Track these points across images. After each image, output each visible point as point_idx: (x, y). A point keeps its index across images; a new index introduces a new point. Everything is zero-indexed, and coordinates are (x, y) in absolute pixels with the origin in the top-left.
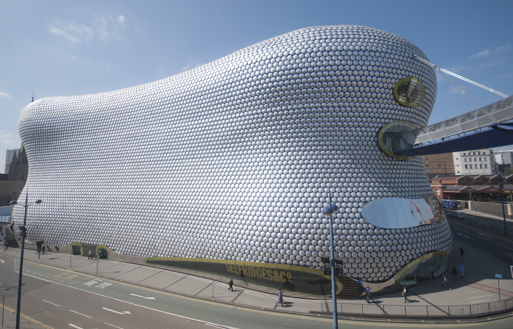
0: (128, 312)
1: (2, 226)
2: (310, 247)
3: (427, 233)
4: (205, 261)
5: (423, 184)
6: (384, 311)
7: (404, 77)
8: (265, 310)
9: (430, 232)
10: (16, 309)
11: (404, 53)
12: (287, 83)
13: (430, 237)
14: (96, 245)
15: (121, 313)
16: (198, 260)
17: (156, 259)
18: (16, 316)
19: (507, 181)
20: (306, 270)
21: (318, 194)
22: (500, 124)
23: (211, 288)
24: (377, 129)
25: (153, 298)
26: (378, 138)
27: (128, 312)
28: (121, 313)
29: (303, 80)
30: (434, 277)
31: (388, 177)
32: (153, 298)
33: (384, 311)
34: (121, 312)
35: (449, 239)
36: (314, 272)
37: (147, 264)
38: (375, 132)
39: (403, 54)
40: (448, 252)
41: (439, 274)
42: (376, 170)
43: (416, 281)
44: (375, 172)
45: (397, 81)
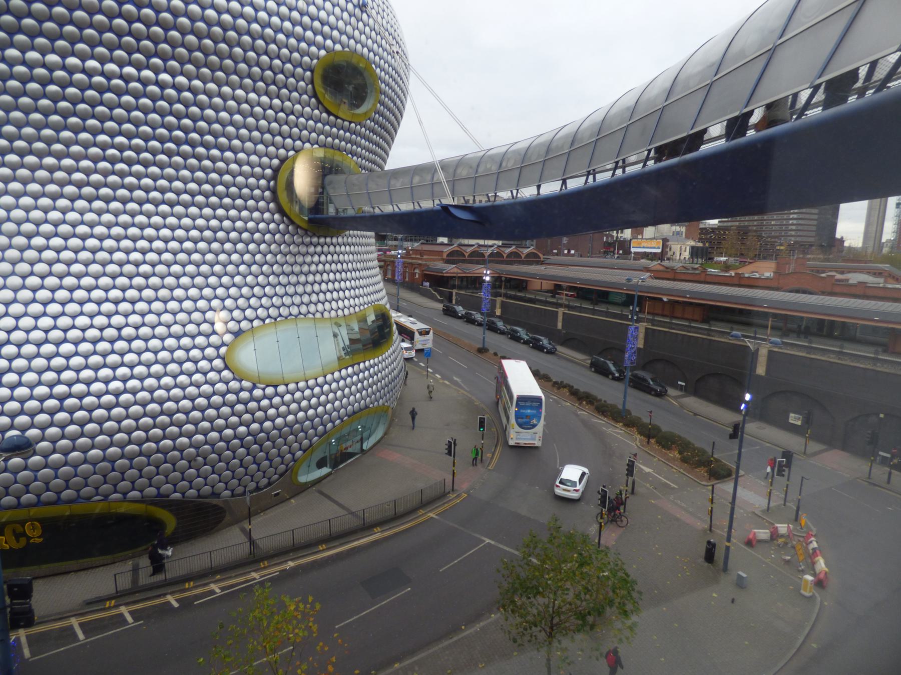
24: (276, 162)
45: (323, 53)
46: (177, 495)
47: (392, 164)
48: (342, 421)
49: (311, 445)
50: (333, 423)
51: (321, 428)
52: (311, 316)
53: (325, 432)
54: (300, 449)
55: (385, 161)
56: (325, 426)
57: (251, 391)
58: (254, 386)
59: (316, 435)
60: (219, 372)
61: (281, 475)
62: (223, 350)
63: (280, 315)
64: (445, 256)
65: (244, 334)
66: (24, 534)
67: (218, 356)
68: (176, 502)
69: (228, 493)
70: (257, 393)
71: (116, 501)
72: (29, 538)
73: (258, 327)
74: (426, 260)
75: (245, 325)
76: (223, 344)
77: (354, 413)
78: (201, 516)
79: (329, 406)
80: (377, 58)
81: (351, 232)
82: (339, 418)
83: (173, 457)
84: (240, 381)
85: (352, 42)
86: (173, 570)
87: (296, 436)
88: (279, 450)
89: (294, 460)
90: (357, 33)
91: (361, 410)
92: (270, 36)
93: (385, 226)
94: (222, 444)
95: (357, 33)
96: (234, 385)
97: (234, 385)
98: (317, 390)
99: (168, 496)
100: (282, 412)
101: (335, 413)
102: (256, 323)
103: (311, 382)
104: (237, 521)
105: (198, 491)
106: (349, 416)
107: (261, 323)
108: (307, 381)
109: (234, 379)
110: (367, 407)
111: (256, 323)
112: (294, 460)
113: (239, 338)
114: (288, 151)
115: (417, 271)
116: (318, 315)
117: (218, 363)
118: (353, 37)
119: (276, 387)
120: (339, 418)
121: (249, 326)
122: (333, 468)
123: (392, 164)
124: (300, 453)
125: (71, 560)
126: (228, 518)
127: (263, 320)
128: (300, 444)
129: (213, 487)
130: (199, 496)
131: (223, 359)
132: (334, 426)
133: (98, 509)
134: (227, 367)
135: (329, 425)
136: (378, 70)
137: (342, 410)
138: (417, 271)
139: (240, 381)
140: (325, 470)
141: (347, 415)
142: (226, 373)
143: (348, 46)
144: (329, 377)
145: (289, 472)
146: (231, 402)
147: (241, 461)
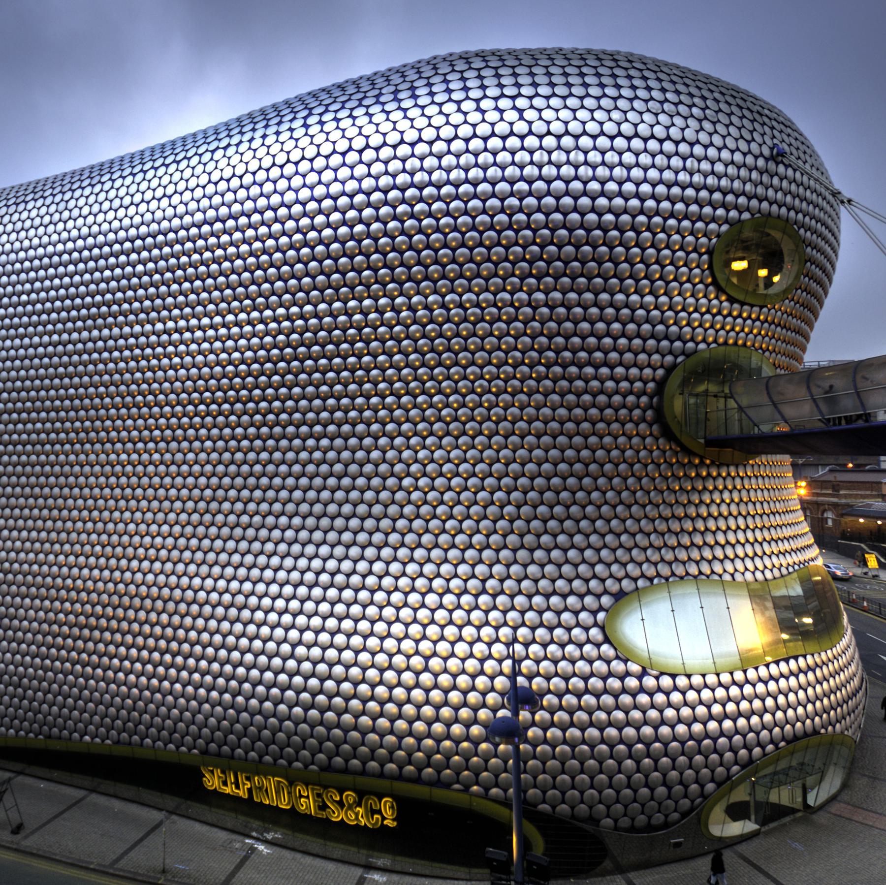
2: (563, 232)
3: (793, 681)
4: (139, 753)
7: (746, 216)
9: (802, 677)
11: (749, 142)
13: (801, 694)
20: (439, 794)
21: (480, 569)
23: (156, 839)
24: (660, 372)
29: (445, 190)
30: (806, 806)
38: (653, 380)
39: (743, 146)
40: (850, 733)
41: (824, 796)
42: (643, 522)
43: (756, 822)
44: (636, 545)
45: (725, 228)
46: (544, 807)
47: (817, 354)
49: (729, 778)
50: (763, 748)
51: (743, 752)
52: (716, 577)
54: (712, 780)
56: (750, 751)
57: (640, 678)
58: (644, 672)
60: (598, 646)
61: (684, 815)
62: (601, 616)
63: (658, 575)
65: (626, 598)
66: (379, 812)
67: (596, 624)
69: (609, 822)
71: (476, 795)
72: (384, 818)
73: (644, 588)
74: (845, 496)
76: (601, 608)
77: (796, 738)
87: (706, 757)
88: (681, 774)
89: (702, 795)
90: (771, 192)
91: (806, 735)
92: (619, 207)
94: (604, 747)
97: (618, 666)
98: (734, 691)
99: (535, 806)
100: (680, 717)
101: (765, 733)
102: (641, 583)
103: (725, 678)
105: (573, 808)
107: (648, 583)
108: (718, 675)
109: (617, 657)
110: (815, 732)
111: (641, 583)
112: (702, 795)
113: (621, 602)
114: (676, 357)
116: (727, 577)
117: (594, 632)
118: (766, 199)
119: (673, 676)
120: (772, 741)
121: (633, 586)
122: (763, 824)
123: (817, 354)
124: (710, 786)
125: (423, 858)
126: (607, 864)
127: (651, 580)
128: (713, 771)
129: (591, 808)
130: (573, 816)
131: (603, 628)
133: (462, 800)
134: (607, 640)
135: (757, 751)
137: (765, 733)
139: (625, 661)
141: (783, 739)
142: (605, 648)
143: (759, 211)
144: (752, 674)
145: (696, 816)
146: (420, 733)
147: (629, 778)
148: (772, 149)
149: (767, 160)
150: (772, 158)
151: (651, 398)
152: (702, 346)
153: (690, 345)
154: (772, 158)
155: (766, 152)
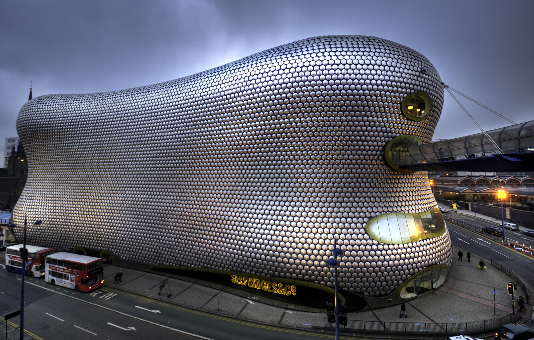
0: (133, 328)
1: (2, 227)
5: (427, 197)
6: (385, 327)
7: (413, 91)
8: (270, 325)
10: (19, 324)
11: (413, 67)
12: (293, 91)
14: (100, 251)
15: (126, 329)
16: (204, 270)
17: (161, 266)
18: (24, 300)
19: (507, 183)
20: (310, 284)
21: (324, 209)
22: (505, 155)
24: (384, 143)
25: (158, 311)
26: (384, 152)
27: (133, 328)
28: (126, 329)
31: (397, 73)
32: (158, 311)
33: (385, 327)
34: (126, 328)
35: (450, 250)
36: (317, 286)
37: (153, 272)
40: (447, 264)
45: (405, 95)
46: (345, 289)
48: (423, 269)
49: (407, 279)
50: (418, 269)
51: (412, 270)
53: (414, 273)
54: (401, 280)
55: (432, 136)
56: (414, 270)
57: (377, 245)
58: (379, 244)
59: (409, 274)
61: (392, 291)
62: (364, 225)
63: (383, 211)
64: (459, 183)
66: (290, 290)
67: (362, 228)
68: (345, 291)
70: (380, 247)
71: (323, 284)
72: (292, 292)
74: (446, 185)
75: (373, 214)
76: (364, 222)
77: (429, 265)
78: (356, 301)
79: (416, 259)
80: (431, 91)
81: (419, 172)
82: (421, 267)
83: (358, 270)
84: (372, 240)
85: (419, 87)
86: (351, 325)
90: (421, 83)
91: (433, 264)
93: (431, 168)
95: (421, 83)
96: (370, 242)
97: (370, 242)
100: (391, 258)
102: (377, 214)
103: (406, 245)
104: (371, 310)
106: (427, 267)
109: (370, 239)
110: (436, 263)
111: (377, 214)
112: (398, 285)
115: (440, 191)
116: (406, 212)
117: (362, 230)
118: (419, 85)
119: (388, 245)
120: (421, 267)
121: (375, 215)
122: (418, 294)
126: (366, 307)
130: (355, 292)
131: (365, 229)
132: (419, 271)
134: (366, 233)
135: (416, 270)
136: (431, 96)
138: (440, 191)
139: (372, 240)
140: (414, 295)
141: (425, 266)
142: (365, 235)
144: (414, 244)
147: (374, 279)
148: (421, 69)
149: (420, 72)
150: (421, 72)
151: (381, 152)
152: (398, 135)
153: (394, 134)
154: (421, 72)
155: (419, 70)
